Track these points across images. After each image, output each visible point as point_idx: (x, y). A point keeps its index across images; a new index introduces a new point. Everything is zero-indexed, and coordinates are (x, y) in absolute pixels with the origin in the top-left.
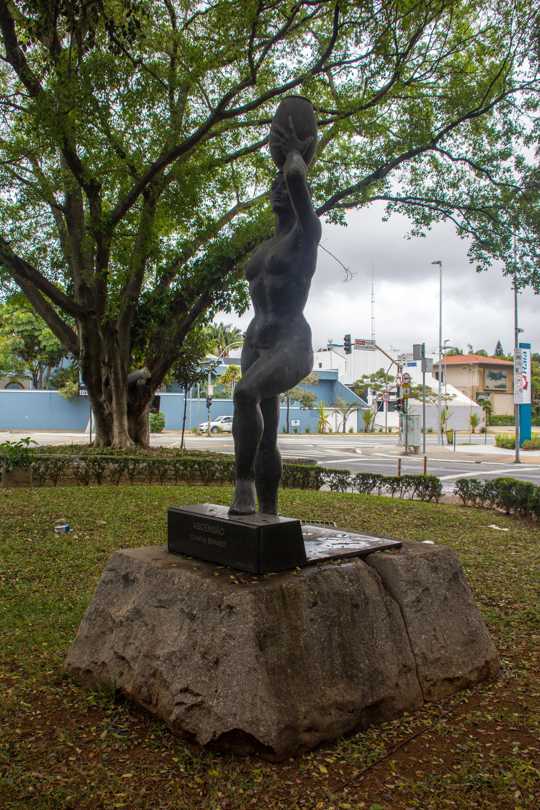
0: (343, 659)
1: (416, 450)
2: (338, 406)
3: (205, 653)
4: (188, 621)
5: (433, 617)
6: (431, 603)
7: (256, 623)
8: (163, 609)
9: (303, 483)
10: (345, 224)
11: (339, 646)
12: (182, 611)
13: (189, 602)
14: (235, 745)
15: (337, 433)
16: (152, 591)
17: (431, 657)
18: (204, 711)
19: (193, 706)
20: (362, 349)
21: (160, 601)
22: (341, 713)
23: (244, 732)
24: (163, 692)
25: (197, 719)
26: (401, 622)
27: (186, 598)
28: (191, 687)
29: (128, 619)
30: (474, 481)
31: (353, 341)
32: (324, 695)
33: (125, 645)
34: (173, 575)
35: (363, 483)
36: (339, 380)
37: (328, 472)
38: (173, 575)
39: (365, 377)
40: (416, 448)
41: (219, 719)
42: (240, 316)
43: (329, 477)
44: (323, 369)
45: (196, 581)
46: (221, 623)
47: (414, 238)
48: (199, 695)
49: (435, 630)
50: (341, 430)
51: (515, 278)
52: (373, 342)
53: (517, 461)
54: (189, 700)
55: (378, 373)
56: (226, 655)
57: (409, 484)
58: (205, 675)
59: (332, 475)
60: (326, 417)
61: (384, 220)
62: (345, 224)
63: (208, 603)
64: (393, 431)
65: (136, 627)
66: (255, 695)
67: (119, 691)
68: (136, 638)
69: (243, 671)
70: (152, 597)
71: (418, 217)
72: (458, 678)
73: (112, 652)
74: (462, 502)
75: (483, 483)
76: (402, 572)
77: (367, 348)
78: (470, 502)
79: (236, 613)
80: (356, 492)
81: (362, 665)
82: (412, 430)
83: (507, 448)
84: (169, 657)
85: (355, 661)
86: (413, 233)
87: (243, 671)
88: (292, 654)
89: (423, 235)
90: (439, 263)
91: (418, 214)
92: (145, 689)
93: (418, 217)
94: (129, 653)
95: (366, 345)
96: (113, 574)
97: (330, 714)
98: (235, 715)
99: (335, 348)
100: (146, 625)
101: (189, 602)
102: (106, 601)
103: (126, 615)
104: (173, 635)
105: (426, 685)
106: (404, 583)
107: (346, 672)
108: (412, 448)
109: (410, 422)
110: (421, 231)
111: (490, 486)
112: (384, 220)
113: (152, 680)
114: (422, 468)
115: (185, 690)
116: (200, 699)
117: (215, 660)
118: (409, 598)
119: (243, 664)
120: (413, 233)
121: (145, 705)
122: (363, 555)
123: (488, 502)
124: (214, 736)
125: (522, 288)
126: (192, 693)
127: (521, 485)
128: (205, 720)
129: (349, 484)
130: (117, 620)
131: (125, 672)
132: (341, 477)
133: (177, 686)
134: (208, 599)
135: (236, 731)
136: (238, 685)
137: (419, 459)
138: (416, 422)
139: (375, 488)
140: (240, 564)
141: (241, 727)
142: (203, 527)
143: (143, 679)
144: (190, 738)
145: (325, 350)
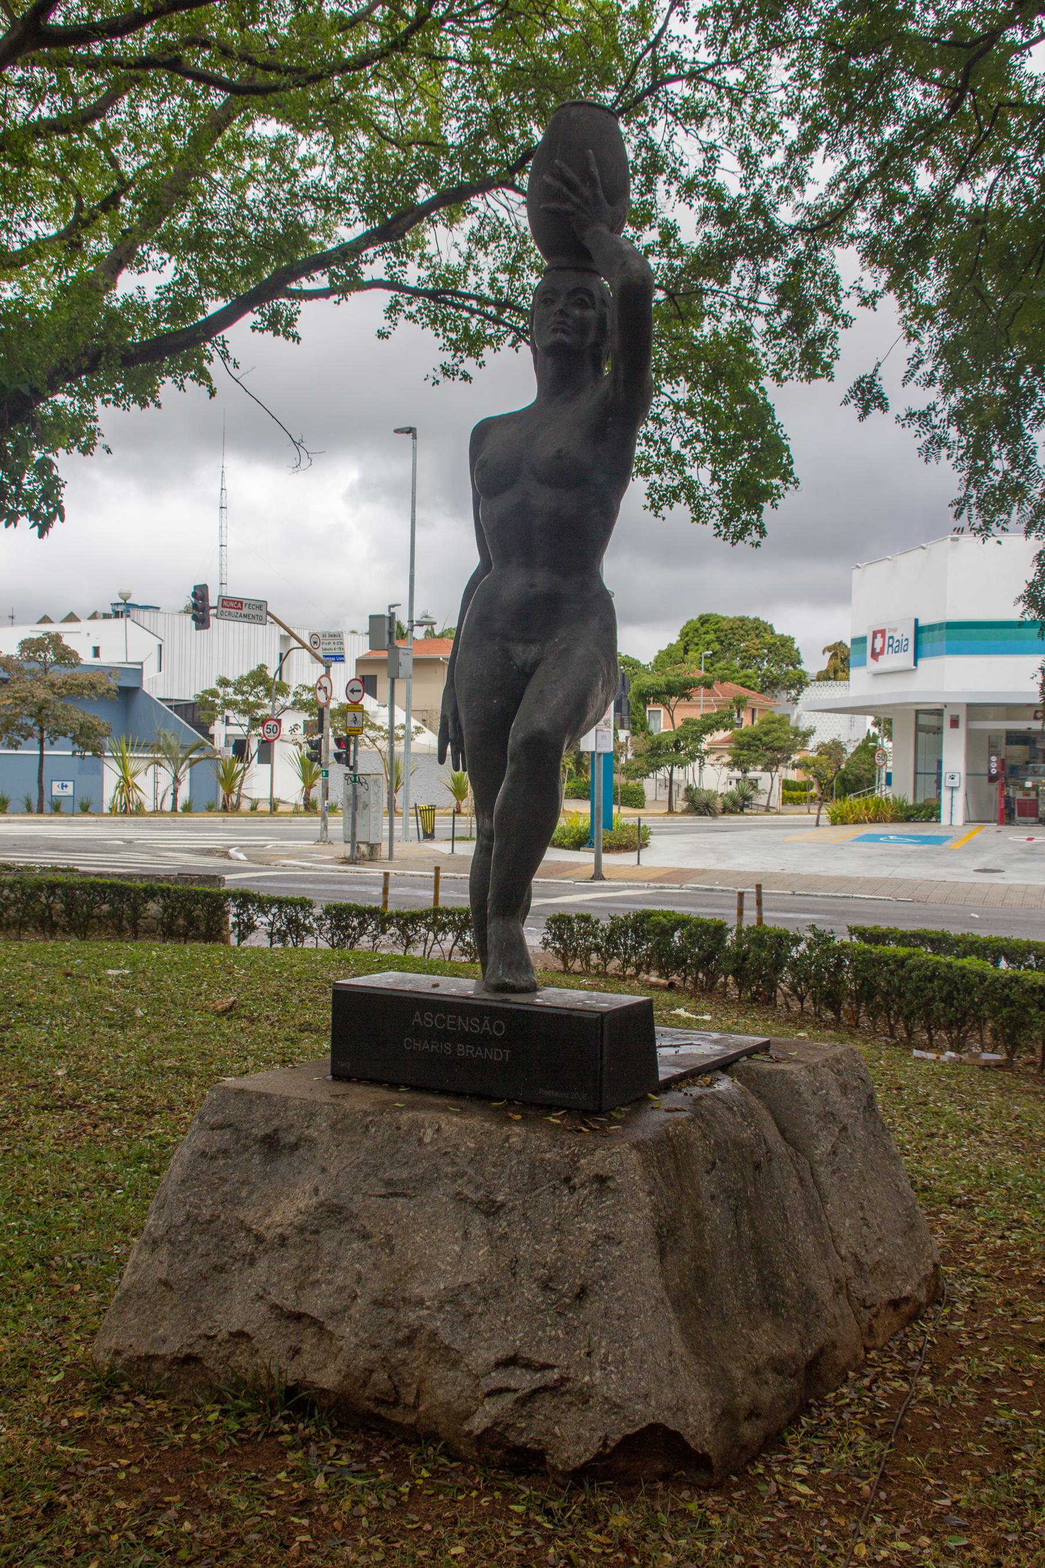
0: (760, 1272)
1: (372, 854)
2: (159, 749)
3: (551, 1279)
4: (478, 1219)
5: (856, 1183)
6: (852, 1157)
7: (655, 1209)
8: (401, 1200)
9: (209, 928)
10: (296, 338)
11: (752, 1247)
12: (460, 1198)
13: (481, 1179)
14: (650, 1458)
15: (158, 812)
16: (365, 1163)
17: (867, 1259)
18: (568, 1398)
19: (535, 1392)
20: (236, 618)
21: (389, 1183)
22: (780, 1378)
23: (666, 1428)
24: (439, 1372)
25: (546, 1418)
26: (816, 1194)
27: (471, 1171)
28: (526, 1353)
29: (301, 1230)
30: (586, 919)
31: (213, 601)
32: (751, 1345)
33: (300, 1287)
34: (416, 1125)
35: (338, 927)
36: (146, 688)
37: (263, 904)
38: (416, 1125)
39: (224, 682)
40: (373, 848)
41: (615, 1408)
42: (41, 535)
43: (266, 914)
44: (105, 660)
45: (488, 1133)
46: (580, 1213)
47: (446, 383)
48: (552, 1367)
49: (862, 1208)
50: (168, 806)
51: (652, 485)
52: (261, 605)
53: (598, 876)
54: (523, 1381)
55: (252, 675)
56: (604, 1278)
57: (442, 928)
58: (555, 1325)
59: (274, 910)
60: (134, 775)
61: (382, 335)
62: (296, 338)
63: (532, 1177)
64: (281, 808)
65: (329, 1246)
66: (671, 1353)
67: (291, 1391)
68: (332, 1268)
69: (648, 1306)
70: (367, 1176)
71: (453, 336)
72: (907, 1299)
73: (262, 1308)
74: (558, 964)
75: (606, 923)
76: (807, 1095)
77: (249, 618)
78: (578, 962)
79: (614, 1191)
80: (324, 945)
81: (788, 1283)
82: (366, 806)
83: (564, 847)
84: (452, 1298)
85: (776, 1275)
86: (446, 371)
87: (648, 1306)
88: (698, 1268)
89: (466, 377)
90: (411, 431)
91: (455, 329)
92: (380, 1377)
93: (453, 336)
94: (315, 1304)
95: (245, 611)
96: (227, 1135)
97: (767, 1383)
98: (646, 1396)
99: (134, 613)
100: (366, 1237)
101: (481, 1179)
102: (218, 1196)
103: (297, 1221)
104: (446, 1254)
105: (866, 1315)
106: (813, 1118)
107: (767, 1298)
108: (364, 848)
109: (361, 790)
110: (462, 367)
111: (619, 928)
112: (382, 335)
113: (401, 1354)
114: (431, 894)
115: (510, 1362)
116: (555, 1374)
117: (577, 1290)
118: (822, 1148)
119: (646, 1294)
120: (446, 371)
121: (383, 1411)
122: (725, 1066)
123: (616, 962)
124: (605, 1445)
125: (666, 508)
126: (528, 1365)
127: (701, 924)
128: (573, 1415)
129: (309, 930)
130: (268, 1236)
131: (306, 1347)
132: (292, 915)
133: (483, 1356)
134: (533, 1165)
135: (654, 1429)
136: (643, 1334)
137: (374, 872)
138: (373, 789)
139: (365, 938)
140: (549, 1094)
141: (661, 1419)
142: (441, 1021)
143: (374, 1355)
144: (527, 1462)
145: (106, 616)
